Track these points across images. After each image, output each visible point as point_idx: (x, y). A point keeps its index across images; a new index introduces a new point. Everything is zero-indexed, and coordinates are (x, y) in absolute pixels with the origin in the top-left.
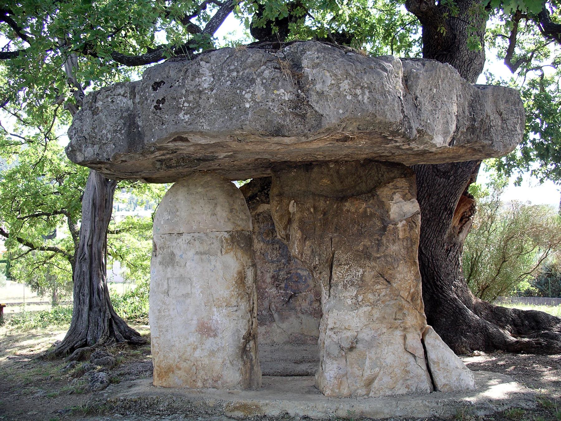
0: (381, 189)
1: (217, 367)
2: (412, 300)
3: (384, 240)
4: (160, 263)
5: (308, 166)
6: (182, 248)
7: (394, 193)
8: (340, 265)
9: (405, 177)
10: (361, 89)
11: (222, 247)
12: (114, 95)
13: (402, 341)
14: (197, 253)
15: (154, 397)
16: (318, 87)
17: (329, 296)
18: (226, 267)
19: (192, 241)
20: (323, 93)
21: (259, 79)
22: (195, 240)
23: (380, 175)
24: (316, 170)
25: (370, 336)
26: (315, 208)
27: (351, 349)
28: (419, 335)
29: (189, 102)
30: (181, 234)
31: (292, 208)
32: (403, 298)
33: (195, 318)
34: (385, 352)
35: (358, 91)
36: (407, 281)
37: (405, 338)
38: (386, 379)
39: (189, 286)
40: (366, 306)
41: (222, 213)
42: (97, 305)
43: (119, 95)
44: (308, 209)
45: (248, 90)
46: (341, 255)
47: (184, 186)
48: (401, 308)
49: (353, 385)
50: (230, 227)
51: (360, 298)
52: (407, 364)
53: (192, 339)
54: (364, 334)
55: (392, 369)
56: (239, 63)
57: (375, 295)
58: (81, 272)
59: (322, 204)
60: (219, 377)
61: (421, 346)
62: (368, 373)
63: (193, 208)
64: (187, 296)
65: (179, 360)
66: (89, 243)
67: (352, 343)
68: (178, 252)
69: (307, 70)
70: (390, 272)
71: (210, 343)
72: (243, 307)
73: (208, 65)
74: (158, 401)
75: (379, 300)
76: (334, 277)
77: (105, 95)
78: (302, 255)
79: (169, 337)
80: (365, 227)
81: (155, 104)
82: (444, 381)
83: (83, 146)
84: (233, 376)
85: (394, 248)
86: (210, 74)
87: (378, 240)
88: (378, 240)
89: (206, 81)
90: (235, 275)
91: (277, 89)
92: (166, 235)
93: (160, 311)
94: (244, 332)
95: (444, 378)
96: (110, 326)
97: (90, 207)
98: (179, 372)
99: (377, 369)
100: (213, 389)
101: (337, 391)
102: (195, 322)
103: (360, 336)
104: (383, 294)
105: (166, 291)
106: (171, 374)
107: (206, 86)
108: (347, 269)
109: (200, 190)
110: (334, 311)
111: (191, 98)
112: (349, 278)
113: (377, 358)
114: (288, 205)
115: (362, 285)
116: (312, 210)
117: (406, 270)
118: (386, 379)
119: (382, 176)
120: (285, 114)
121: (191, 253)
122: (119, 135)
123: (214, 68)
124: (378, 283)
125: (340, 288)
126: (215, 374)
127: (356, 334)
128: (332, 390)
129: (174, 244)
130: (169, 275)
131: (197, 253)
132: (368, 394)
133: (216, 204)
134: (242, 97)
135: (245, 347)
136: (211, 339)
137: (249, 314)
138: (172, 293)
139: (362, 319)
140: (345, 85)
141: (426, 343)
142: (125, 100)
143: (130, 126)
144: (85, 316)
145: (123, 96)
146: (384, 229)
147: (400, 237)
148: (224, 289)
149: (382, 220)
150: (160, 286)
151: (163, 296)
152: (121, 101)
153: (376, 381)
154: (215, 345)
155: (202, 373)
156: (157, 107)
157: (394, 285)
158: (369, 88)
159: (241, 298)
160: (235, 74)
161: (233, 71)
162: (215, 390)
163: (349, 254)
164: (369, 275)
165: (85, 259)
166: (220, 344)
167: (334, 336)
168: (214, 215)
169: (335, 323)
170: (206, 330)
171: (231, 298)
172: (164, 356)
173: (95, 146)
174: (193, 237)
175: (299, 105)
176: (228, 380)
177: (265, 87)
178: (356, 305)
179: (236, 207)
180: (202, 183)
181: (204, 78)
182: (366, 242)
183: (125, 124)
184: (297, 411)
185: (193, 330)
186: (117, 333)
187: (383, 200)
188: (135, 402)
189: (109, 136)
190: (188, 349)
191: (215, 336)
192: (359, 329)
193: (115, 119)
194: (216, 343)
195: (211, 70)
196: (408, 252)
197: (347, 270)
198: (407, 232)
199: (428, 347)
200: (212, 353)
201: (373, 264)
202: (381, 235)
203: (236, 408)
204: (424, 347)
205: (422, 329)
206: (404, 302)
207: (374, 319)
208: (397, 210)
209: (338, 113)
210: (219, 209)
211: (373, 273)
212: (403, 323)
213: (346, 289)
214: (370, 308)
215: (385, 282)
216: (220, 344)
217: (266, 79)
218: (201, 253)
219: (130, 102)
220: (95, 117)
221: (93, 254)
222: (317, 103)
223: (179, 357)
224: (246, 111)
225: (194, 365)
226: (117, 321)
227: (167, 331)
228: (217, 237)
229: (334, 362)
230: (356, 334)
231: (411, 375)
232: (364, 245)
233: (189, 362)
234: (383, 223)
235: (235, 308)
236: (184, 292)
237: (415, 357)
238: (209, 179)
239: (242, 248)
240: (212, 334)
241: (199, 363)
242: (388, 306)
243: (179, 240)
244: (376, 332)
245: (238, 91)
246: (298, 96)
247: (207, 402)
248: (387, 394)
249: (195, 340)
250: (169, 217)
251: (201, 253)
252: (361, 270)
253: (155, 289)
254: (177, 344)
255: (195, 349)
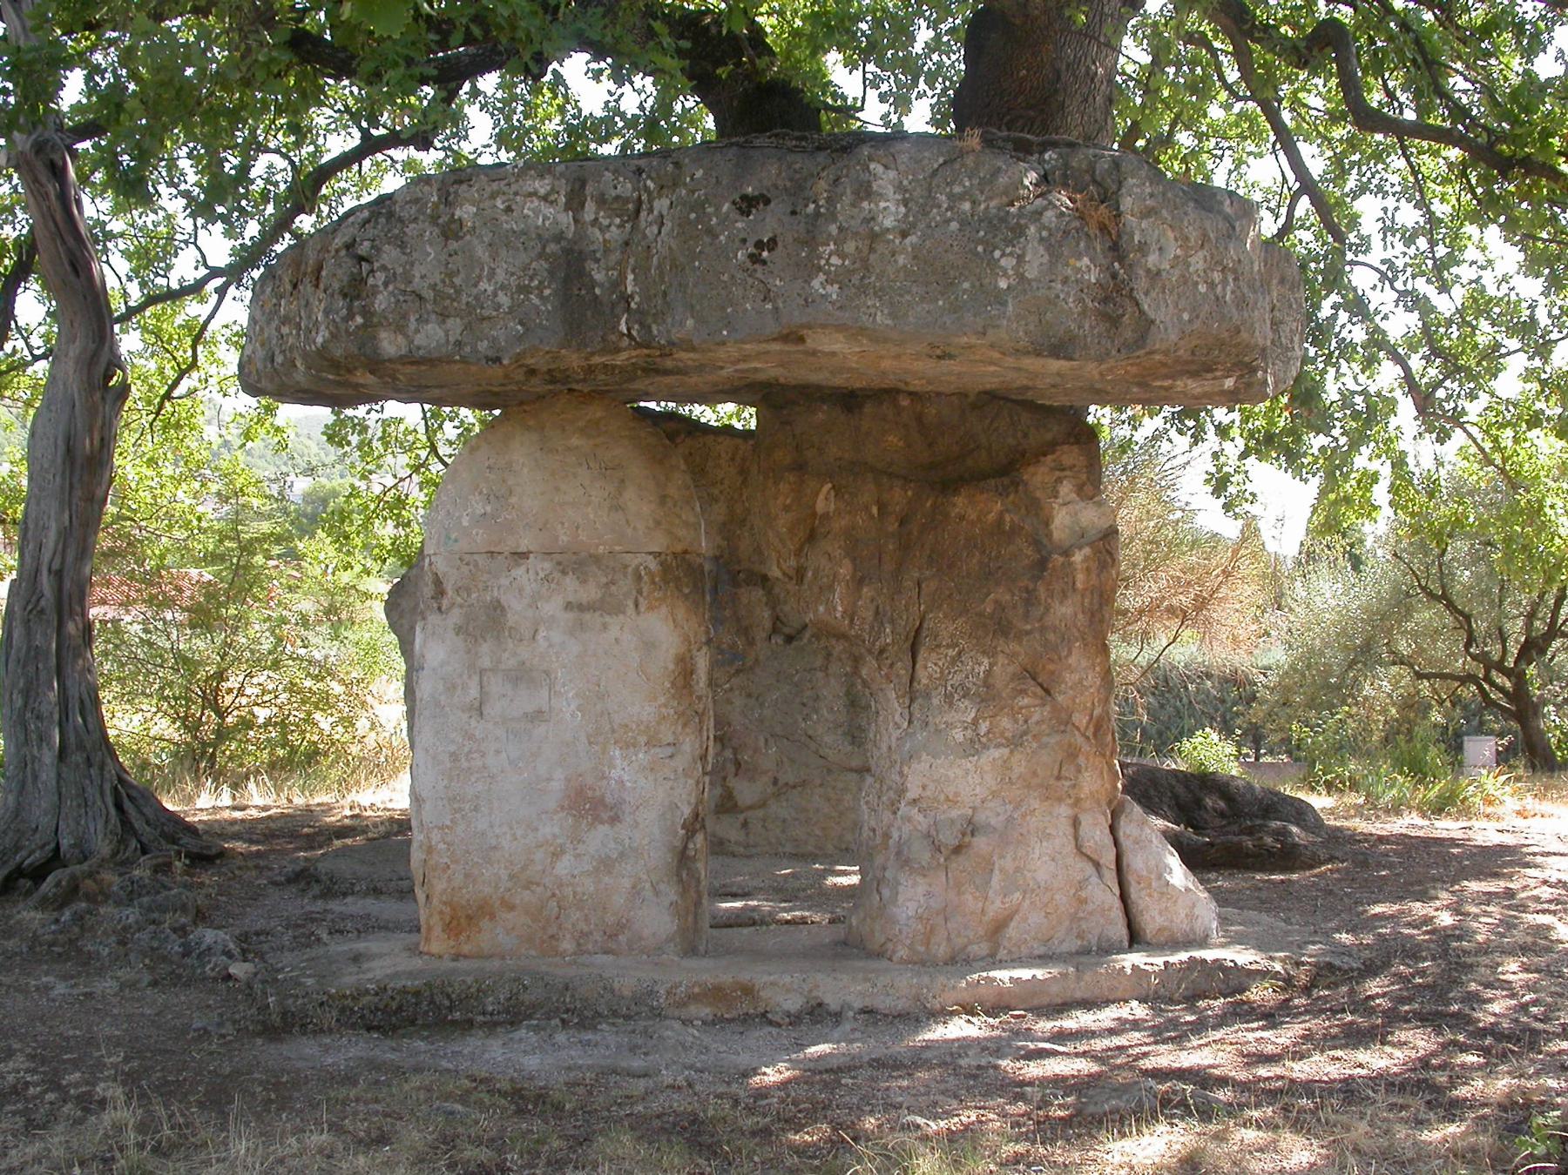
0: (1031, 469)
1: (619, 901)
2: (1095, 735)
3: (1042, 592)
4: (459, 630)
5: (849, 400)
6: (528, 590)
7: (1059, 480)
8: (938, 646)
9: (1077, 442)
10: (1223, 271)
11: (640, 592)
12: (516, 194)
13: (1070, 830)
14: (569, 606)
15: (469, 980)
16: (1152, 259)
17: (910, 722)
18: (649, 646)
19: (557, 575)
20: (1159, 273)
21: (1033, 229)
22: (564, 572)
23: (1019, 435)
24: (868, 409)
25: (1001, 818)
26: (882, 507)
27: (957, 850)
28: (1105, 814)
29: (843, 256)
30: (524, 555)
31: (824, 501)
32: (1078, 729)
33: (559, 774)
34: (1036, 856)
35: (1217, 277)
36: (1087, 688)
37: (1076, 823)
38: (1036, 918)
39: (545, 693)
40: (997, 746)
41: (640, 506)
42: (81, 747)
43: (534, 194)
44: (867, 508)
45: (1008, 250)
46: (944, 626)
47: (528, 428)
48: (1072, 754)
49: (959, 935)
50: (659, 543)
51: (984, 727)
52: (1081, 885)
53: (547, 830)
54: (988, 813)
55: (1049, 894)
56: (975, 182)
57: (1016, 721)
58: (29, 649)
59: (899, 497)
60: (621, 927)
61: (1108, 840)
62: (996, 907)
63: (557, 489)
64: (538, 716)
65: (509, 885)
66: (56, 566)
67: (964, 834)
68: (516, 607)
69: (1130, 219)
70: (1051, 667)
71: (599, 838)
72: (687, 747)
73: (892, 174)
74: (478, 991)
75: (1025, 733)
76: (922, 675)
77: (488, 189)
78: (852, 620)
79: (482, 825)
80: (997, 557)
81: (751, 250)
82: (1160, 920)
83: (412, 319)
84: (656, 920)
85: (1063, 610)
86: (899, 197)
87: (1028, 591)
88: (1028, 591)
89: (889, 212)
90: (671, 667)
91: (1079, 257)
92: (476, 557)
93: (454, 757)
94: (687, 811)
95: (1160, 914)
96: (119, 806)
97: (59, 461)
98: (510, 916)
99: (1018, 895)
100: (605, 957)
101: (922, 949)
102: (557, 785)
103: (981, 817)
104: (1036, 717)
105: (477, 704)
106: (485, 923)
107: (888, 222)
108: (953, 658)
109: (575, 441)
110: (924, 756)
111: (850, 247)
112: (959, 677)
113: (1017, 870)
114: (817, 495)
115: (987, 696)
116: (875, 510)
117: (1084, 663)
118: (1036, 918)
119: (1025, 435)
120: (1083, 313)
121: (552, 607)
122: (536, 301)
123: (905, 182)
124: (1023, 692)
125: (935, 701)
126: (610, 919)
127: (970, 812)
128: (911, 947)
129: (504, 581)
130: (486, 662)
131: (569, 606)
132: (992, 955)
133: (623, 481)
134: (993, 264)
135: (685, 847)
136: (603, 829)
137: (699, 766)
138: (494, 709)
139: (988, 777)
140: (1198, 262)
141: (1121, 834)
142: (549, 211)
143: (567, 281)
144: (48, 775)
145: (545, 198)
146: (1042, 564)
147: (1079, 585)
148: (641, 702)
149: (1036, 543)
150: (459, 691)
151: (465, 717)
152: (537, 212)
153: (1013, 924)
154: (613, 845)
155: (576, 915)
156: (755, 259)
157: (1060, 698)
158: (1234, 271)
159: (685, 725)
160: (967, 206)
161: (961, 197)
162: (611, 957)
163: (960, 621)
164: (1003, 670)
165: (42, 611)
166: (627, 841)
167: (920, 818)
168: (617, 508)
169: (924, 787)
170: (590, 805)
171: (659, 723)
172: (467, 876)
173: (450, 322)
174: (559, 563)
175: (1114, 297)
176: (646, 932)
177: (1047, 249)
178: (974, 746)
179: (672, 491)
180: (581, 424)
181: (882, 204)
182: (1001, 594)
183: (551, 273)
184: (848, 998)
185: (552, 805)
186: (138, 824)
187: (1038, 494)
188: (417, 994)
189: (503, 299)
190: (539, 855)
191: (615, 820)
192: (978, 803)
193: (523, 257)
194: (615, 840)
195: (900, 188)
196: (1091, 622)
197: (953, 661)
198: (1094, 576)
199: (1126, 843)
200: (606, 865)
201: (1014, 646)
202: (1036, 579)
203: (692, 998)
204: (1116, 843)
205: (1110, 803)
206: (1080, 740)
207: (1014, 777)
208: (1068, 520)
209: (1180, 318)
210: (630, 494)
211: (1011, 669)
212: (1074, 786)
213: (951, 704)
214: (1006, 751)
215: (1039, 690)
216: (627, 841)
217: (1050, 230)
218: (581, 608)
219: (566, 219)
220: (453, 245)
221: (66, 598)
222: (1146, 294)
223: (511, 877)
224: (999, 298)
225: (554, 895)
226: (134, 793)
227: (476, 809)
228: (626, 567)
229: (920, 880)
230: (970, 812)
231: (1090, 907)
232: (996, 602)
233: (539, 890)
234: (1039, 551)
235: (670, 750)
236: (530, 709)
237: (1097, 866)
238: (599, 414)
239: (686, 596)
240: (605, 816)
241: (568, 891)
242: (1045, 746)
243: (519, 572)
244: (1016, 808)
245: (980, 249)
246: (1114, 276)
247: (616, 986)
248: (1036, 952)
249: (557, 830)
250: (488, 509)
251: (581, 608)
252: (986, 661)
253: (443, 698)
254: (505, 843)
255: (557, 855)
